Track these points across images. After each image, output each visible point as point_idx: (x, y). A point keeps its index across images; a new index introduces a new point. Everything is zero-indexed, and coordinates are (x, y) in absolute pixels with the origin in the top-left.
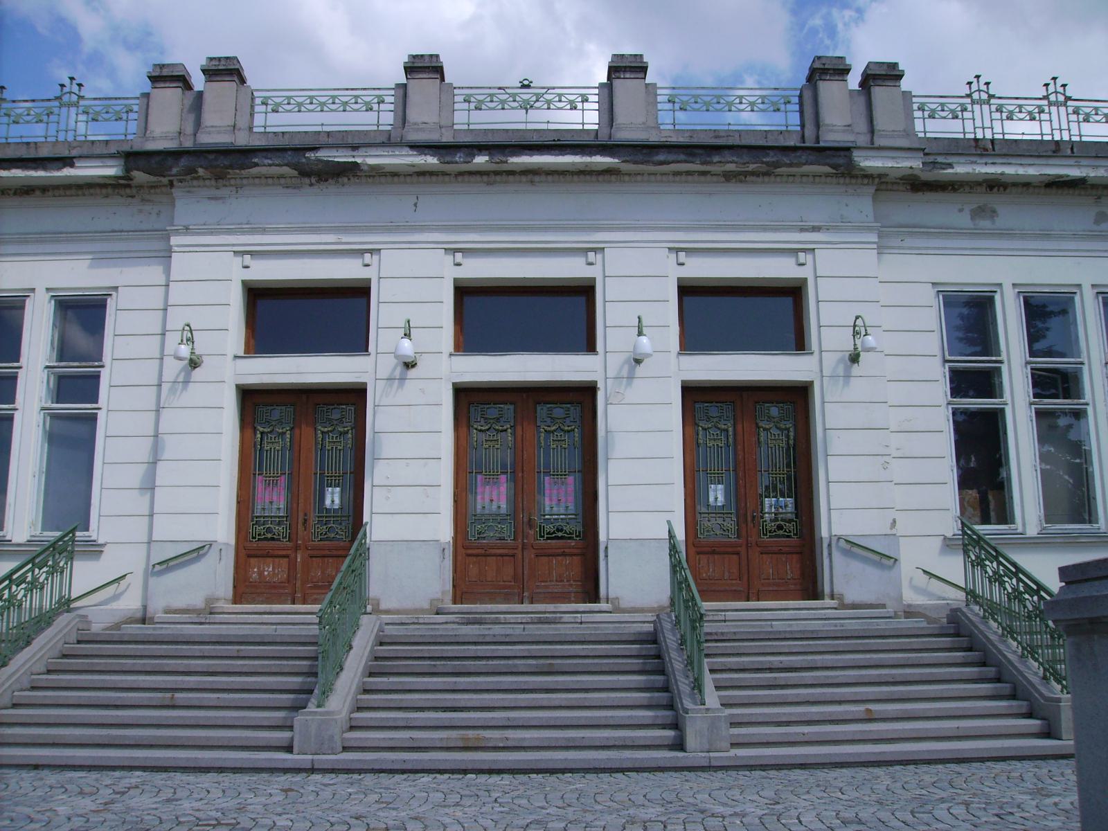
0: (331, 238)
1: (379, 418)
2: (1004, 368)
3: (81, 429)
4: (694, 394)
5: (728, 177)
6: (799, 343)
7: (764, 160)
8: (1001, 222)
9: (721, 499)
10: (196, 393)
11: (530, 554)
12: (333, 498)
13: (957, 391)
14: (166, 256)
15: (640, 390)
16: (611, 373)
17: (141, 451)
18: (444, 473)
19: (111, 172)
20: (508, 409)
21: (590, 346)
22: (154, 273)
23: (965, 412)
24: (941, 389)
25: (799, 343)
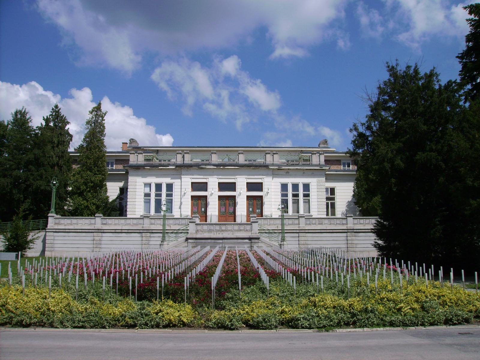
0: (202, 176)
1: (265, 200)
2: (288, 194)
3: (149, 201)
4: (248, 197)
5: (253, 169)
6: (206, 190)
7: (444, 166)
8: (290, 174)
9: (251, 210)
10: (185, 197)
11: (228, 217)
12: (203, 209)
13: (334, 198)
14: (181, 178)
15: (241, 197)
16: (238, 194)
17: (179, 203)
18: (217, 206)
19: (174, 168)
20: (225, 199)
21: (262, 191)
22: (179, 180)
23: (283, 199)
24: (280, 196)
25: (206, 190)
